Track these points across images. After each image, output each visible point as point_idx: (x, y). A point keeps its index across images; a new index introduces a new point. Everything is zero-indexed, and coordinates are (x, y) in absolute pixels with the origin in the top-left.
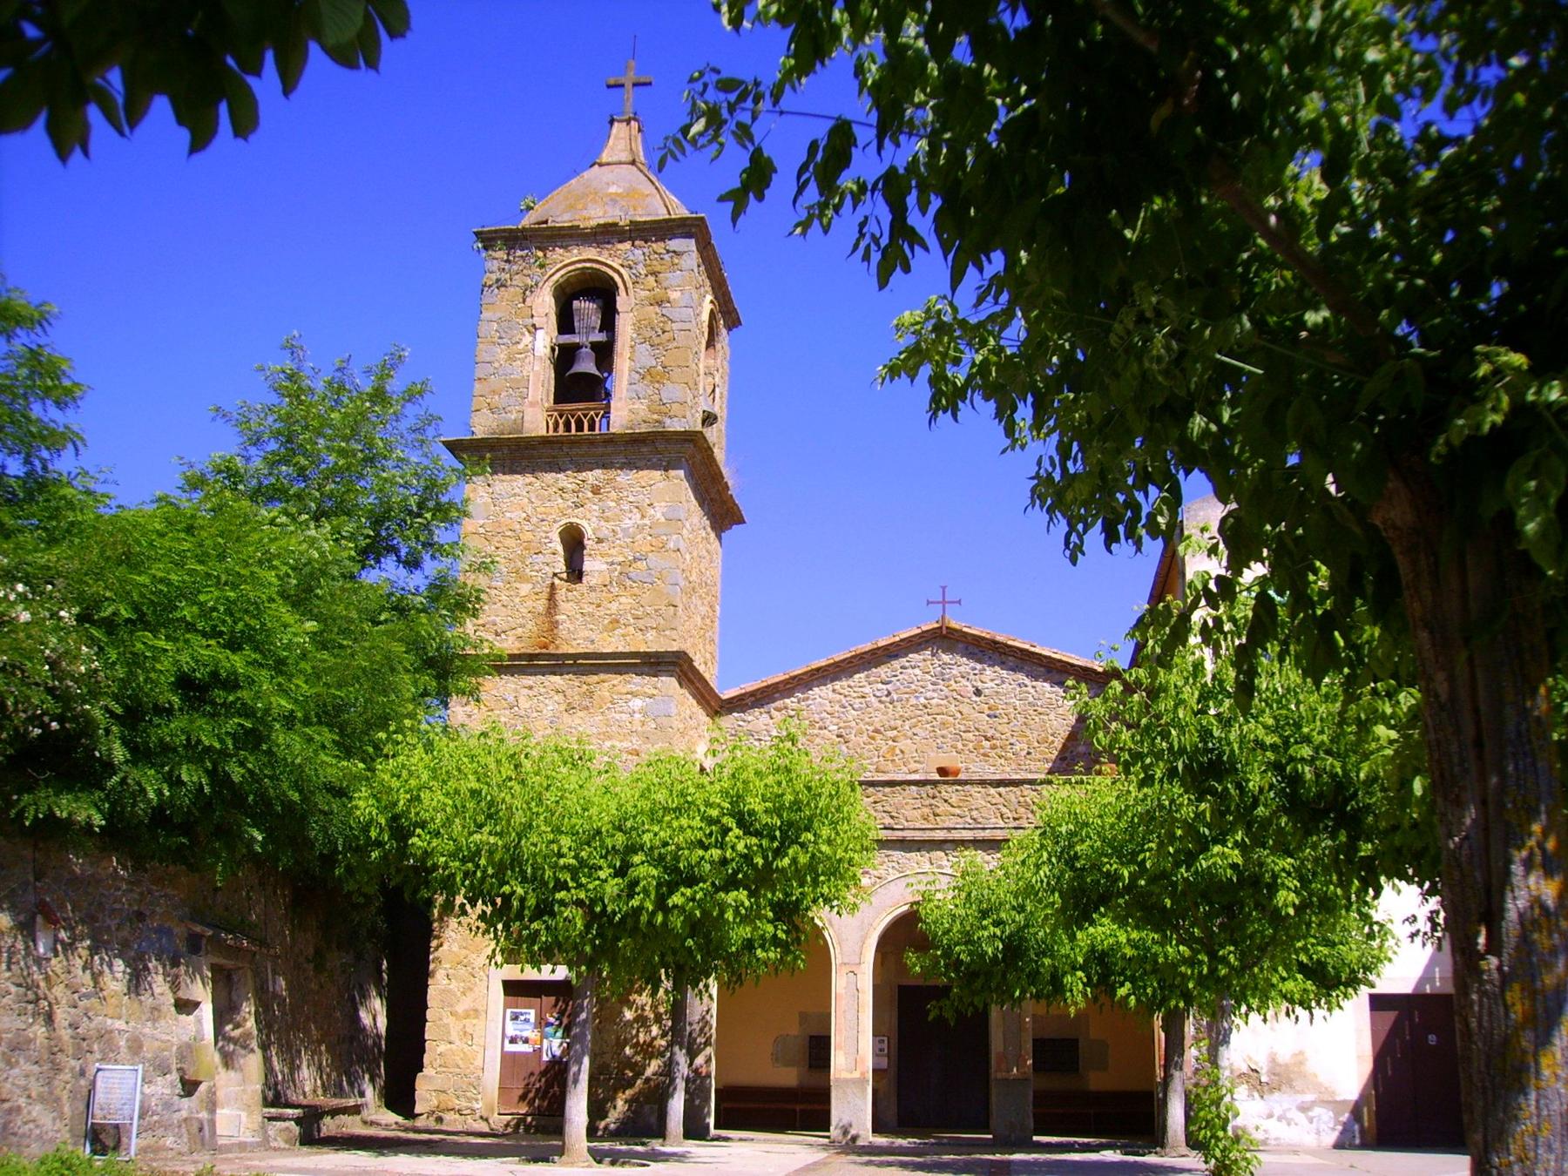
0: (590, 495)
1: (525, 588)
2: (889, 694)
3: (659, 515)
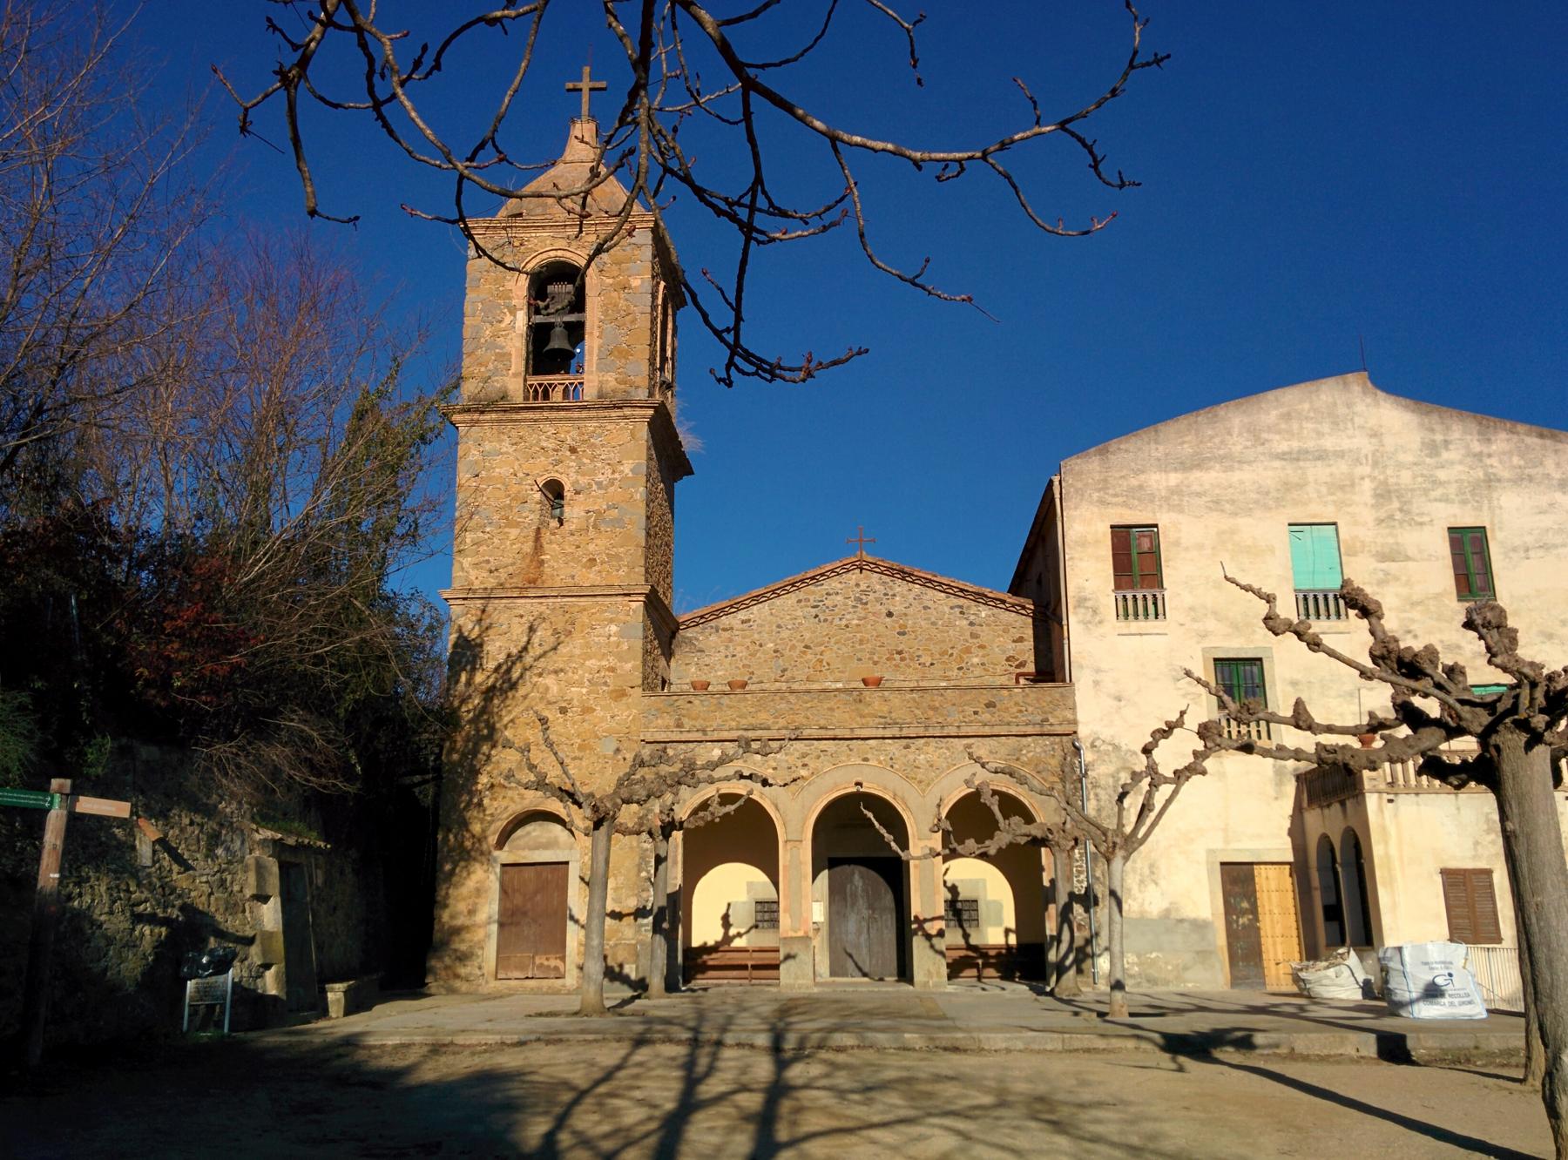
1: (514, 532)
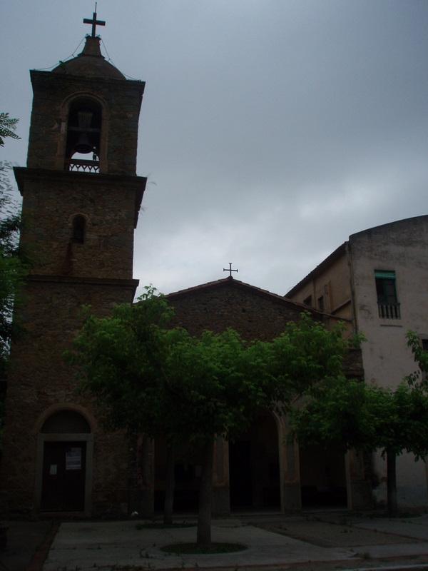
0: (89, 202)
1: (55, 245)
2: (205, 309)
3: (123, 215)
